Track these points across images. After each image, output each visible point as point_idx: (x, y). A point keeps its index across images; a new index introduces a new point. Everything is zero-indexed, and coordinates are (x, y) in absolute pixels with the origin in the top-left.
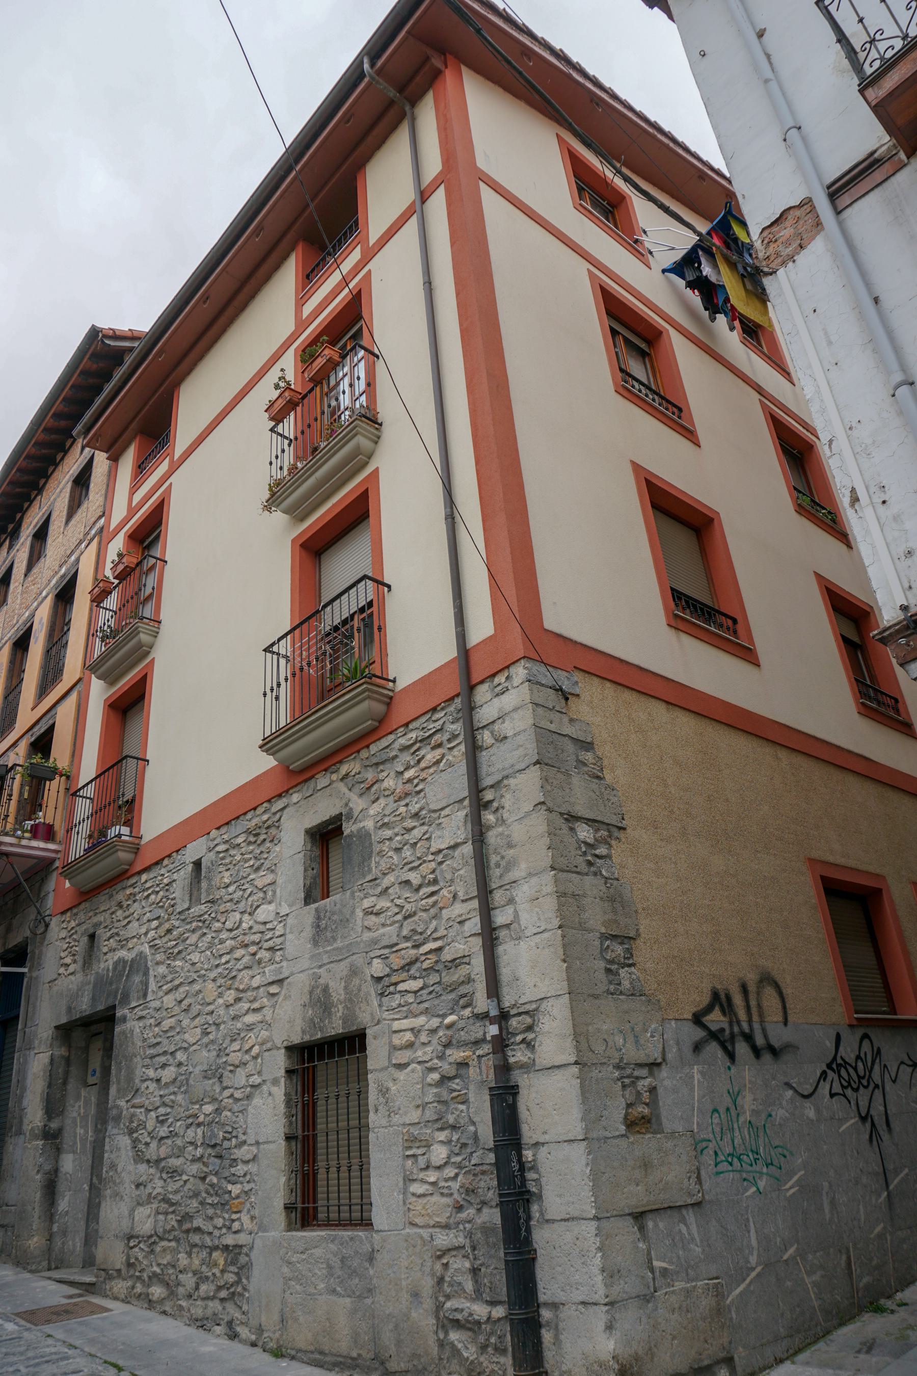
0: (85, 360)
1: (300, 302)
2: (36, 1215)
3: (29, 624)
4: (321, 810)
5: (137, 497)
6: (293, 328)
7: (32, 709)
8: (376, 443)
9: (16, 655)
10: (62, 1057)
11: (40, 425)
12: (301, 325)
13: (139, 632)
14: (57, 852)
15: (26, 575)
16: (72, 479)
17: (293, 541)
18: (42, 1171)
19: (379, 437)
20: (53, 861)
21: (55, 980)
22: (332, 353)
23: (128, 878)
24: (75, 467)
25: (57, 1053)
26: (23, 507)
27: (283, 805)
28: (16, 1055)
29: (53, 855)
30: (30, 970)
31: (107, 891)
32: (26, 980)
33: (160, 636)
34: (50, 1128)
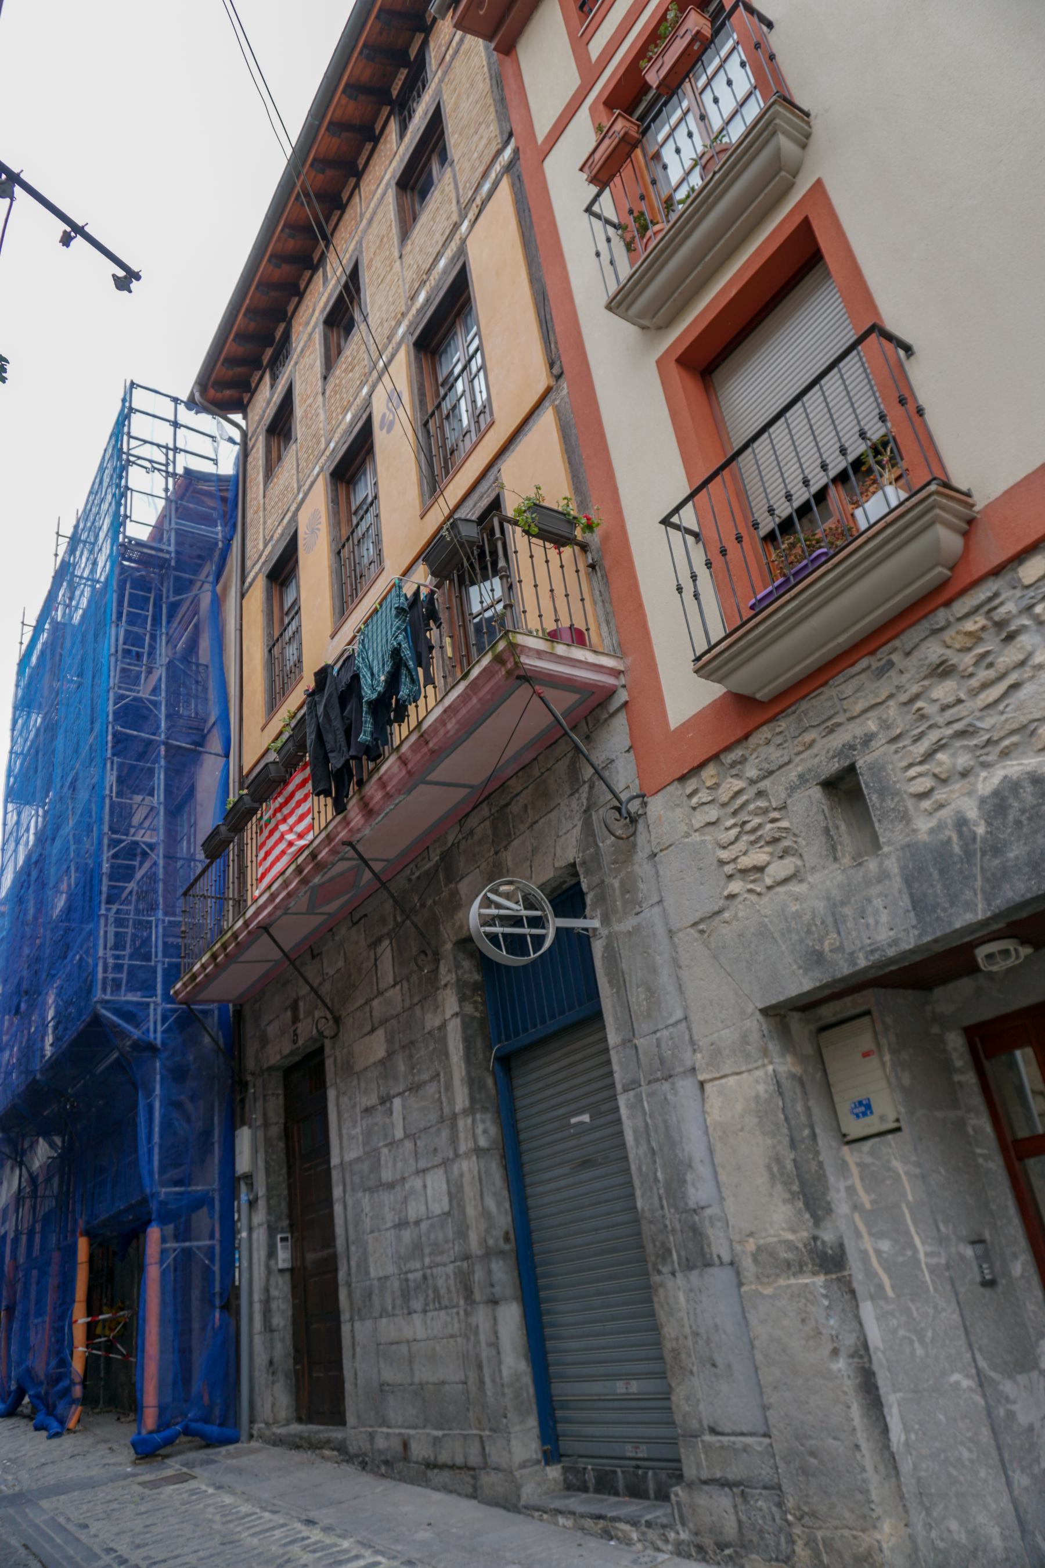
0: (370, 22)
1: (579, 43)
2: (868, 1464)
3: (365, 417)
4: (822, 756)
5: (596, 48)
6: (578, 82)
7: (263, 729)
8: (804, 146)
9: (337, 496)
10: (792, 1076)
11: (323, 117)
12: (589, 72)
13: (774, 133)
14: (617, 673)
15: (325, 378)
16: (322, 320)
17: (659, 362)
18: (843, 1352)
19: (808, 136)
20: (612, 692)
21: (719, 912)
22: (628, 125)
23: (948, 604)
24: (394, 163)
25: (782, 1069)
26: (286, 312)
27: (989, 594)
28: (622, 1101)
29: (611, 681)
30: (606, 920)
31: (863, 663)
32: (598, 948)
33: (813, 138)
34: (824, 1243)
